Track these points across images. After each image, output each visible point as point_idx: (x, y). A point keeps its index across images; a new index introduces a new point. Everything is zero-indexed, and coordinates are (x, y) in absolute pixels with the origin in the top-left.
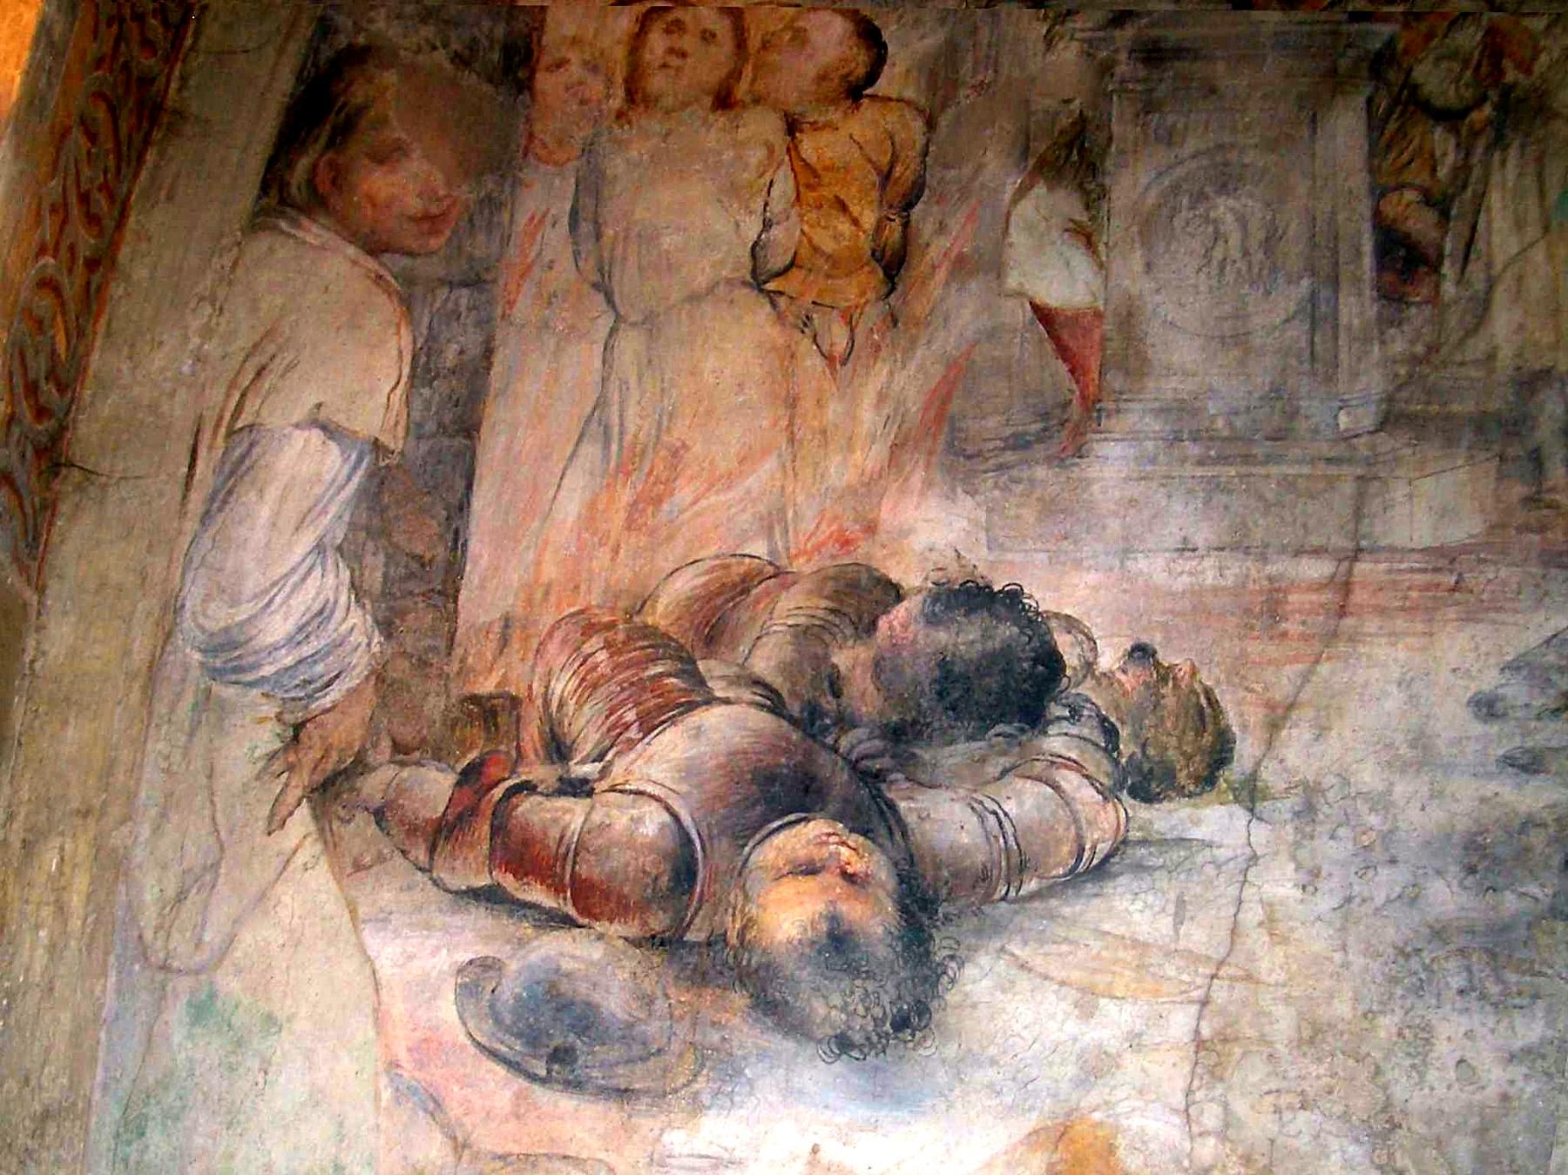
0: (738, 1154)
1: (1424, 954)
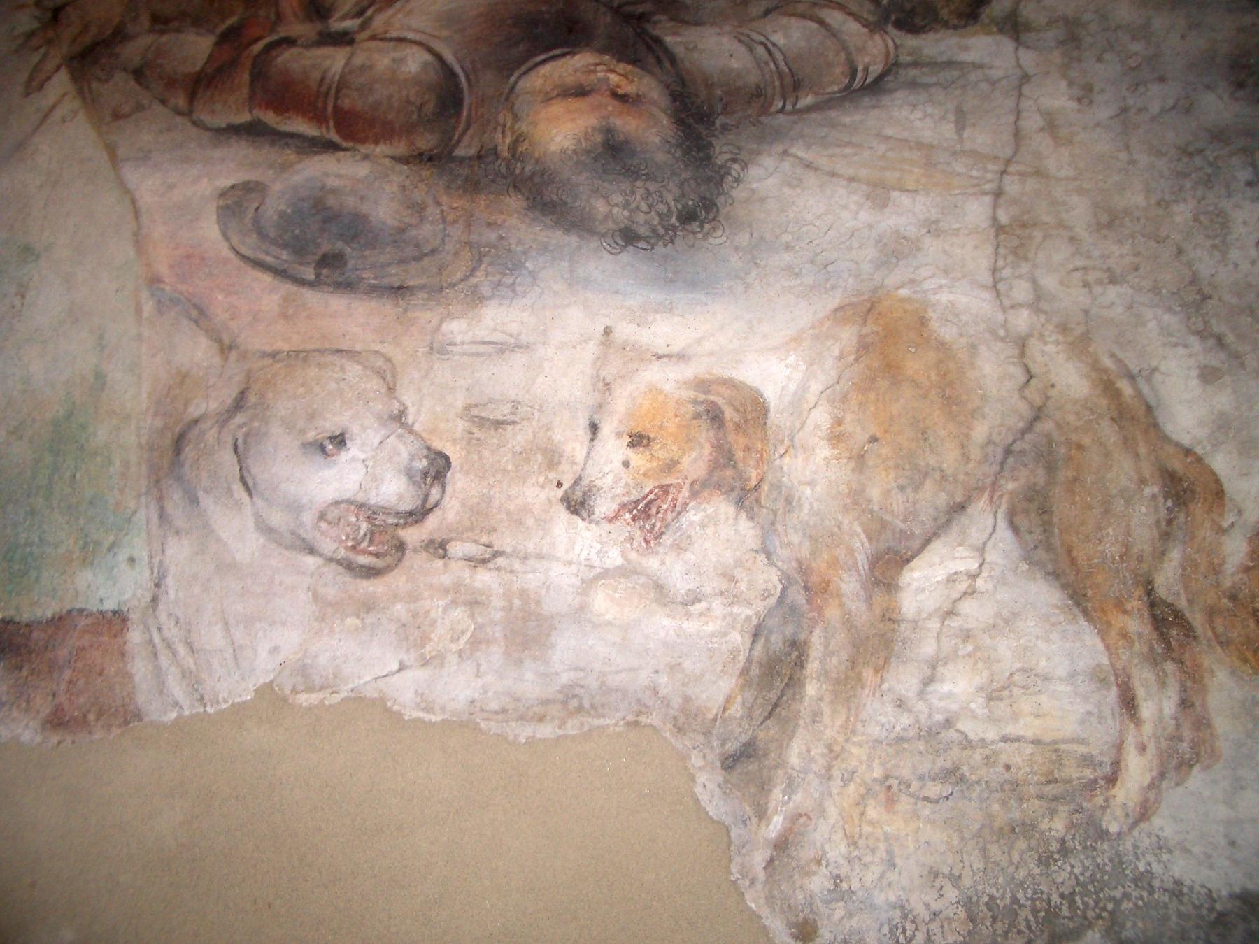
0: (524, 339)
1: (1208, 153)
